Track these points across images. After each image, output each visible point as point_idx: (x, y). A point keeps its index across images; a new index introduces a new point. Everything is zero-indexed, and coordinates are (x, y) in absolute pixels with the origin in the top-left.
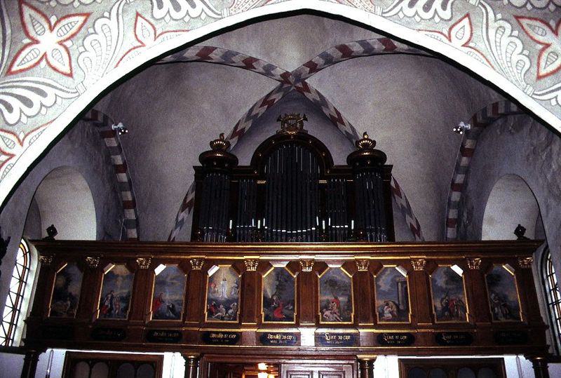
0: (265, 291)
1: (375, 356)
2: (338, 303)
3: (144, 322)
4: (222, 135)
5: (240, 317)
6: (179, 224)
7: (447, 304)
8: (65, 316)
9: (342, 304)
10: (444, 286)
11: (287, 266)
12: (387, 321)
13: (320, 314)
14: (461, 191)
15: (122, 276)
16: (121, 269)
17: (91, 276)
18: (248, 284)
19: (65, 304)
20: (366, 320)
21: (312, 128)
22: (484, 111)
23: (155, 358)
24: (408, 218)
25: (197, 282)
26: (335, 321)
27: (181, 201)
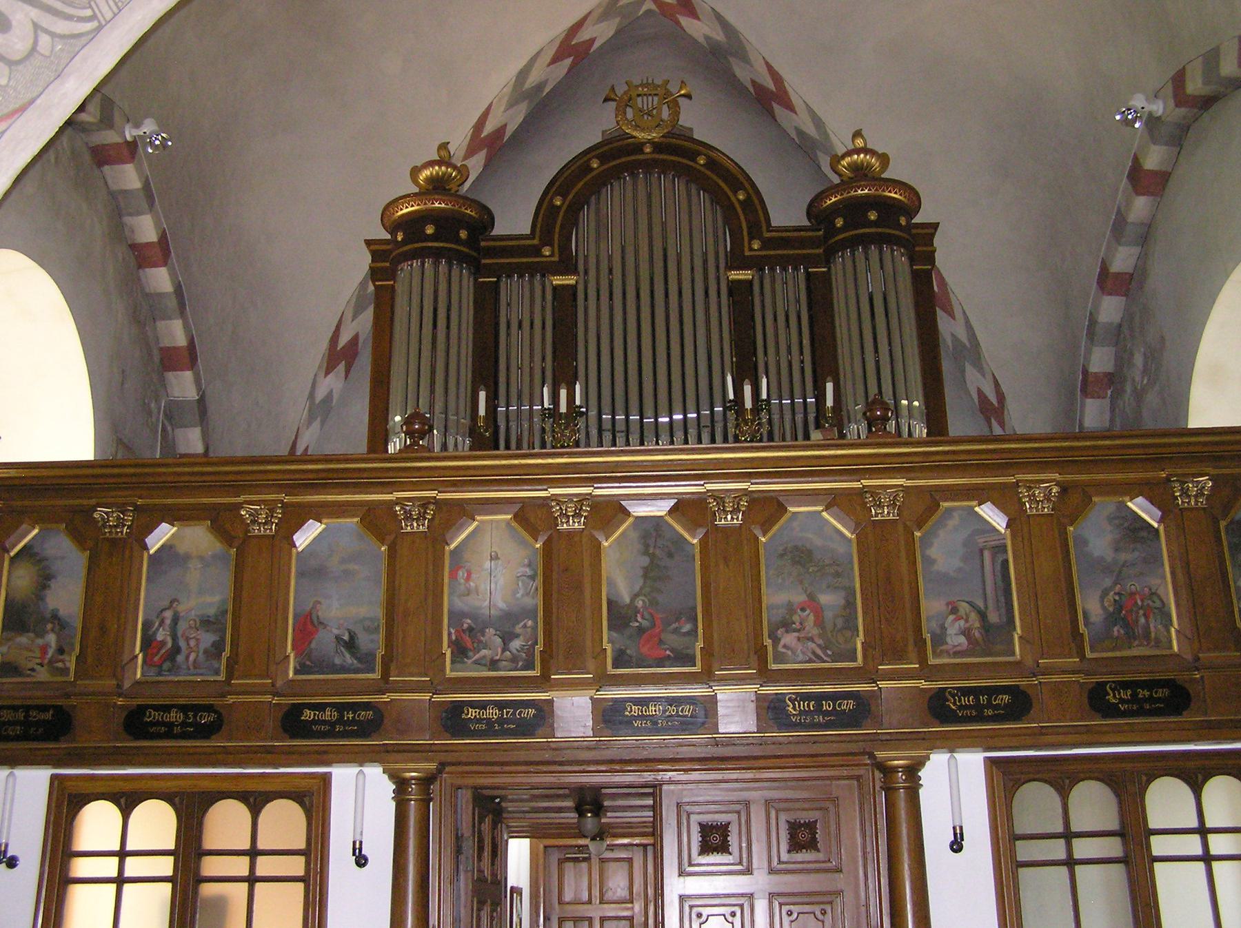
0: (611, 583)
1: (923, 753)
2: (818, 611)
3: (119, 686)
4: (444, 146)
5: (542, 661)
6: (321, 410)
7: (1119, 606)
8: (43, 675)
9: (828, 615)
10: (1109, 555)
11: (671, 512)
12: (957, 654)
13: (768, 642)
14: (1125, 295)
15: (201, 558)
16: (199, 538)
17: (112, 558)
18: (563, 567)
19: (40, 641)
20: (899, 656)
21: (707, 122)
22: (1212, 59)
23: (304, 783)
24: (970, 370)
25: (416, 558)
26: (810, 661)
27: (324, 345)
